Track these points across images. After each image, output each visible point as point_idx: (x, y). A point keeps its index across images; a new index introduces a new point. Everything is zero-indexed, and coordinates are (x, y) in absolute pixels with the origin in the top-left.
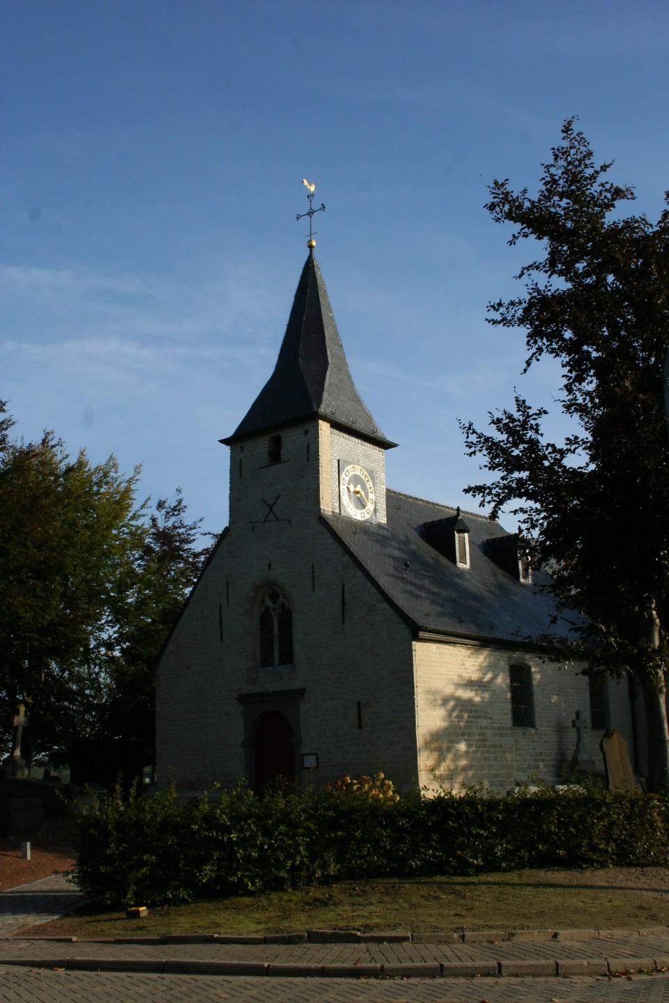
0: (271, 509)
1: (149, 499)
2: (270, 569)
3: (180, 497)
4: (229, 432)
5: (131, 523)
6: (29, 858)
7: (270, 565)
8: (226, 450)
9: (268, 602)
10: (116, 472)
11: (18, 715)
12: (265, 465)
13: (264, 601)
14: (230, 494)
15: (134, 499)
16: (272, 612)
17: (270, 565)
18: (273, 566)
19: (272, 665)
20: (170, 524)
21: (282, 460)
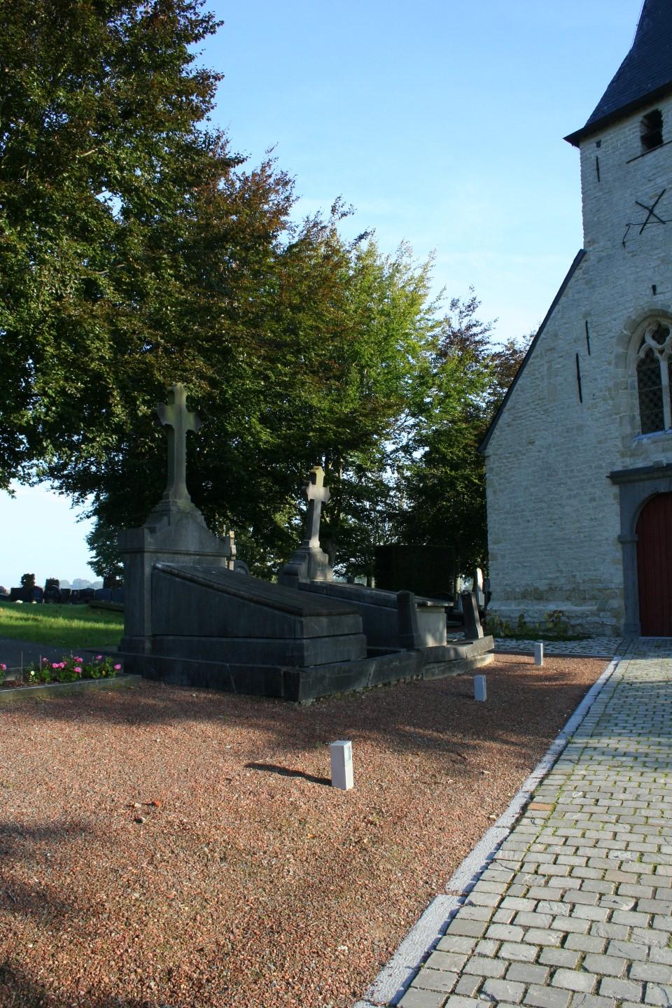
0: (651, 212)
1: (445, 289)
2: (655, 293)
3: (473, 295)
4: (580, 123)
5: (427, 316)
6: (350, 783)
7: (654, 288)
8: (574, 153)
9: (651, 342)
10: (410, 256)
11: (314, 483)
12: (639, 155)
13: (643, 341)
14: (583, 207)
15: (428, 288)
16: (657, 354)
17: (654, 288)
18: (658, 290)
19: (662, 429)
20: (464, 326)
21: (665, 142)
